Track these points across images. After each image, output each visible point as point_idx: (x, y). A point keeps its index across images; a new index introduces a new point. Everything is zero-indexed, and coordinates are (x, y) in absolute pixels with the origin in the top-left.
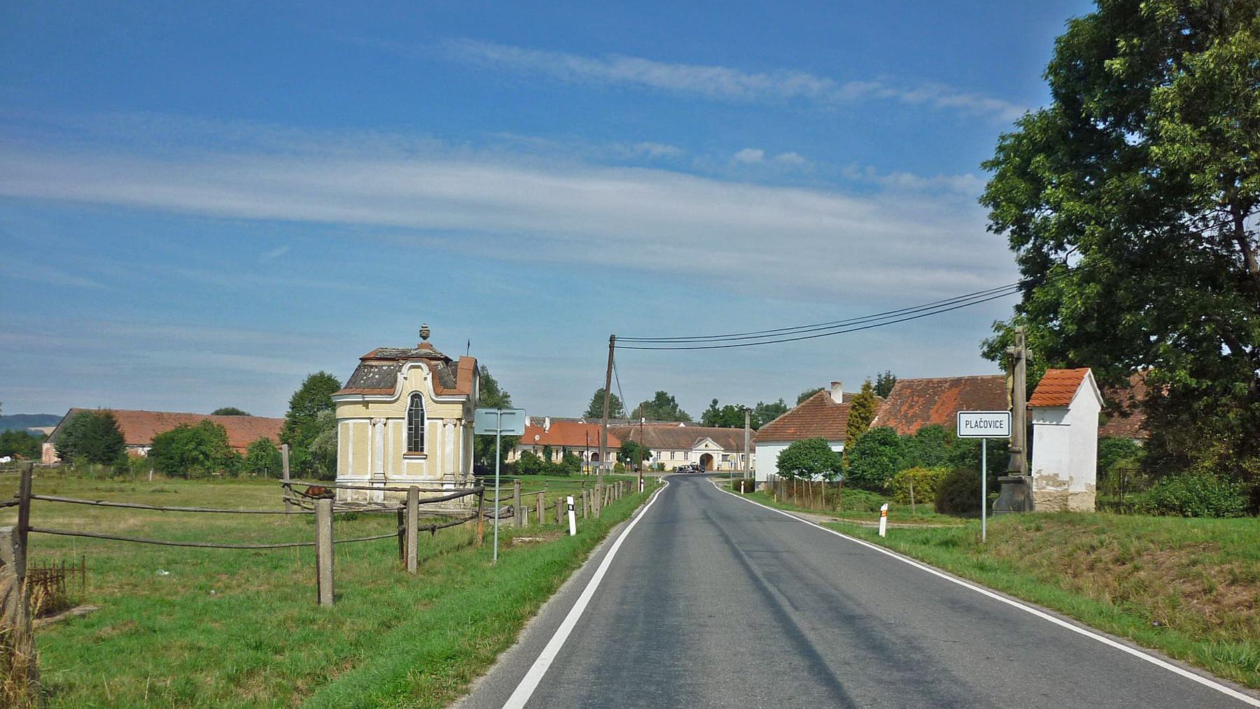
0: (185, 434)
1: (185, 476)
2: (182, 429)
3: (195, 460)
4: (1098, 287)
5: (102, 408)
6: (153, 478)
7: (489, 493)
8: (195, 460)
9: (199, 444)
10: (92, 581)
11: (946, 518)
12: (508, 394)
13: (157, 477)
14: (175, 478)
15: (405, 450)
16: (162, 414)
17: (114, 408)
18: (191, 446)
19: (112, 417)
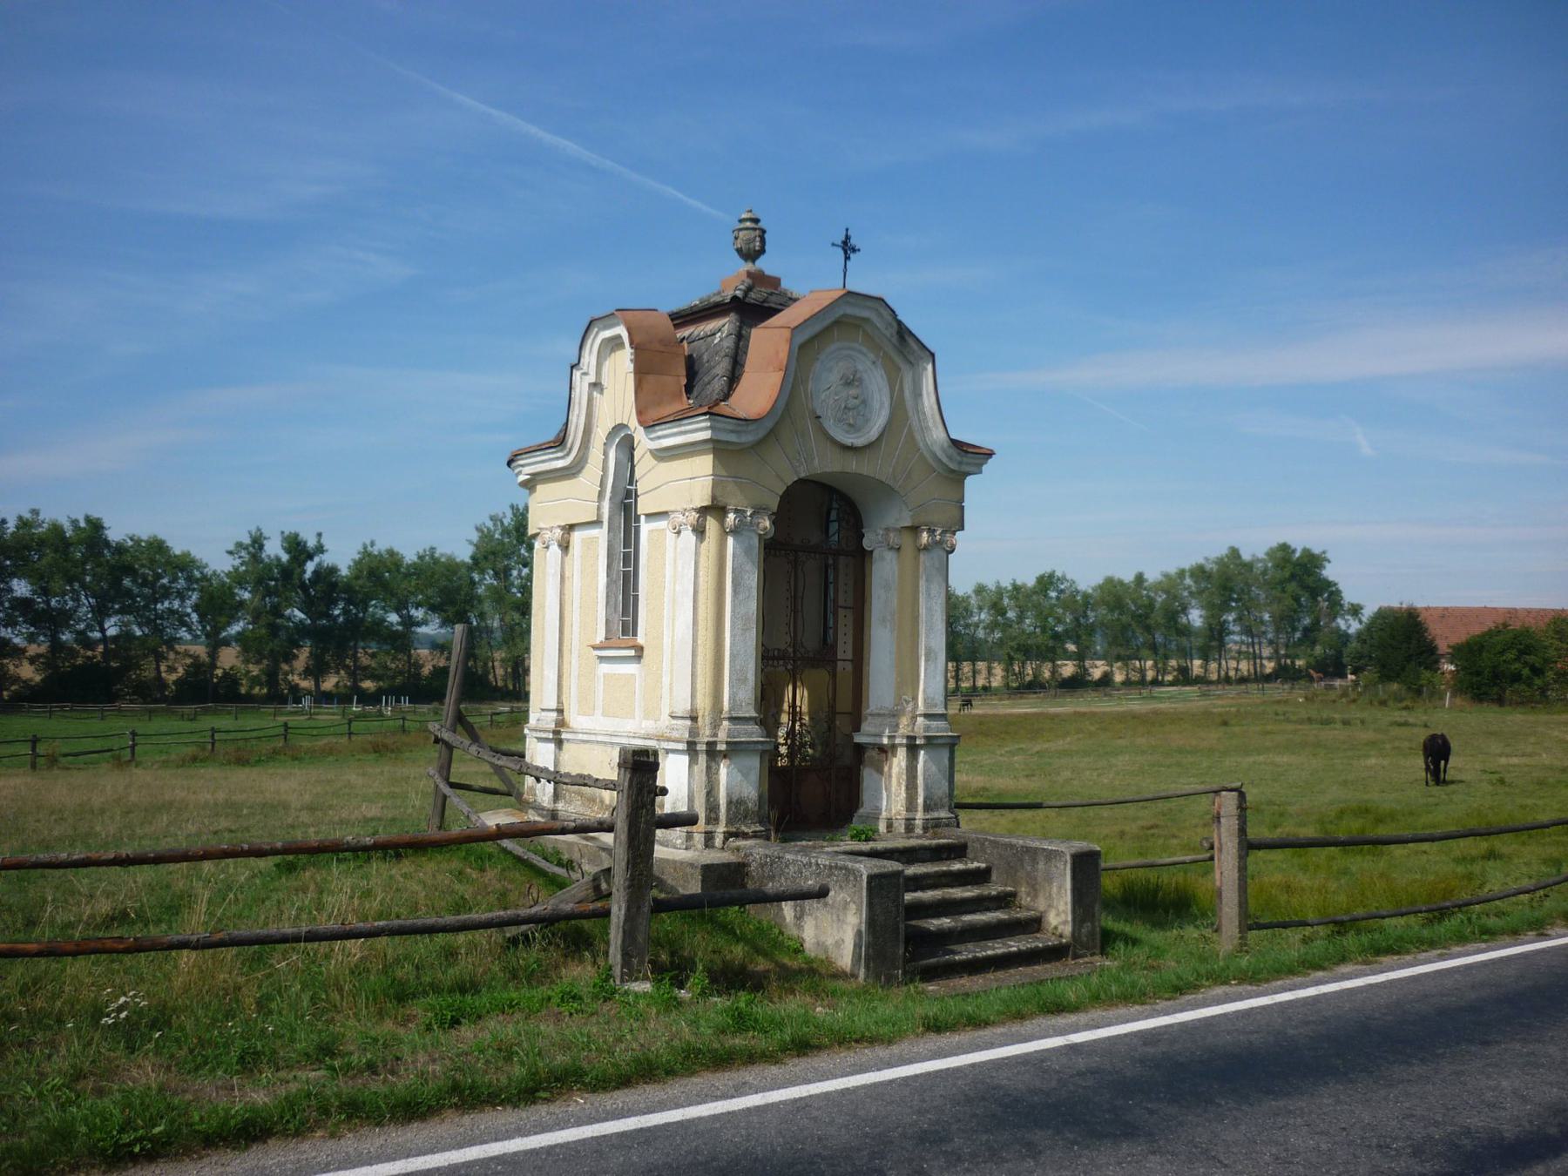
0: (1500, 638)
1: (1500, 701)
2: (1500, 630)
3: (1516, 678)
4: (595, 393)
5: (1404, 606)
6: (1450, 703)
7: (675, 735)
8: (1516, 678)
9: (1522, 652)
10: (449, 899)
11: (899, 994)
12: (247, 541)
13: (1458, 701)
14: (1486, 704)
15: (600, 637)
16: (1516, 610)
17: (1420, 604)
18: (1510, 655)
19: (1418, 616)
